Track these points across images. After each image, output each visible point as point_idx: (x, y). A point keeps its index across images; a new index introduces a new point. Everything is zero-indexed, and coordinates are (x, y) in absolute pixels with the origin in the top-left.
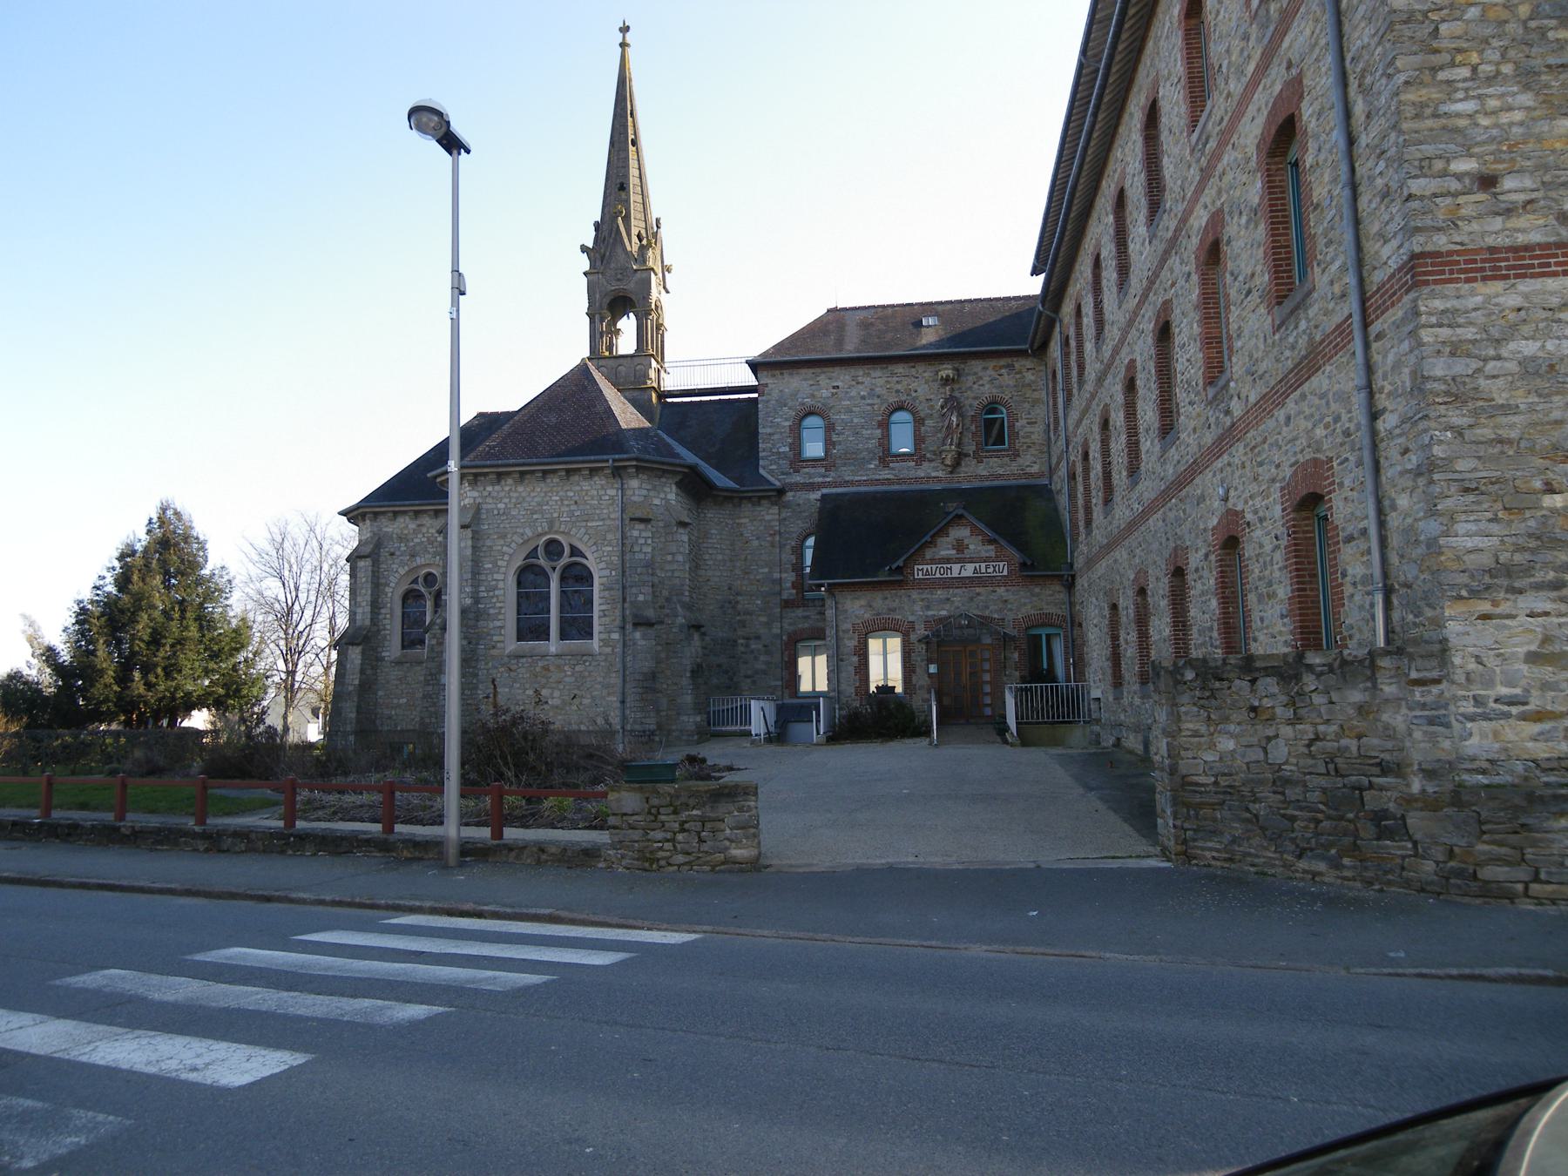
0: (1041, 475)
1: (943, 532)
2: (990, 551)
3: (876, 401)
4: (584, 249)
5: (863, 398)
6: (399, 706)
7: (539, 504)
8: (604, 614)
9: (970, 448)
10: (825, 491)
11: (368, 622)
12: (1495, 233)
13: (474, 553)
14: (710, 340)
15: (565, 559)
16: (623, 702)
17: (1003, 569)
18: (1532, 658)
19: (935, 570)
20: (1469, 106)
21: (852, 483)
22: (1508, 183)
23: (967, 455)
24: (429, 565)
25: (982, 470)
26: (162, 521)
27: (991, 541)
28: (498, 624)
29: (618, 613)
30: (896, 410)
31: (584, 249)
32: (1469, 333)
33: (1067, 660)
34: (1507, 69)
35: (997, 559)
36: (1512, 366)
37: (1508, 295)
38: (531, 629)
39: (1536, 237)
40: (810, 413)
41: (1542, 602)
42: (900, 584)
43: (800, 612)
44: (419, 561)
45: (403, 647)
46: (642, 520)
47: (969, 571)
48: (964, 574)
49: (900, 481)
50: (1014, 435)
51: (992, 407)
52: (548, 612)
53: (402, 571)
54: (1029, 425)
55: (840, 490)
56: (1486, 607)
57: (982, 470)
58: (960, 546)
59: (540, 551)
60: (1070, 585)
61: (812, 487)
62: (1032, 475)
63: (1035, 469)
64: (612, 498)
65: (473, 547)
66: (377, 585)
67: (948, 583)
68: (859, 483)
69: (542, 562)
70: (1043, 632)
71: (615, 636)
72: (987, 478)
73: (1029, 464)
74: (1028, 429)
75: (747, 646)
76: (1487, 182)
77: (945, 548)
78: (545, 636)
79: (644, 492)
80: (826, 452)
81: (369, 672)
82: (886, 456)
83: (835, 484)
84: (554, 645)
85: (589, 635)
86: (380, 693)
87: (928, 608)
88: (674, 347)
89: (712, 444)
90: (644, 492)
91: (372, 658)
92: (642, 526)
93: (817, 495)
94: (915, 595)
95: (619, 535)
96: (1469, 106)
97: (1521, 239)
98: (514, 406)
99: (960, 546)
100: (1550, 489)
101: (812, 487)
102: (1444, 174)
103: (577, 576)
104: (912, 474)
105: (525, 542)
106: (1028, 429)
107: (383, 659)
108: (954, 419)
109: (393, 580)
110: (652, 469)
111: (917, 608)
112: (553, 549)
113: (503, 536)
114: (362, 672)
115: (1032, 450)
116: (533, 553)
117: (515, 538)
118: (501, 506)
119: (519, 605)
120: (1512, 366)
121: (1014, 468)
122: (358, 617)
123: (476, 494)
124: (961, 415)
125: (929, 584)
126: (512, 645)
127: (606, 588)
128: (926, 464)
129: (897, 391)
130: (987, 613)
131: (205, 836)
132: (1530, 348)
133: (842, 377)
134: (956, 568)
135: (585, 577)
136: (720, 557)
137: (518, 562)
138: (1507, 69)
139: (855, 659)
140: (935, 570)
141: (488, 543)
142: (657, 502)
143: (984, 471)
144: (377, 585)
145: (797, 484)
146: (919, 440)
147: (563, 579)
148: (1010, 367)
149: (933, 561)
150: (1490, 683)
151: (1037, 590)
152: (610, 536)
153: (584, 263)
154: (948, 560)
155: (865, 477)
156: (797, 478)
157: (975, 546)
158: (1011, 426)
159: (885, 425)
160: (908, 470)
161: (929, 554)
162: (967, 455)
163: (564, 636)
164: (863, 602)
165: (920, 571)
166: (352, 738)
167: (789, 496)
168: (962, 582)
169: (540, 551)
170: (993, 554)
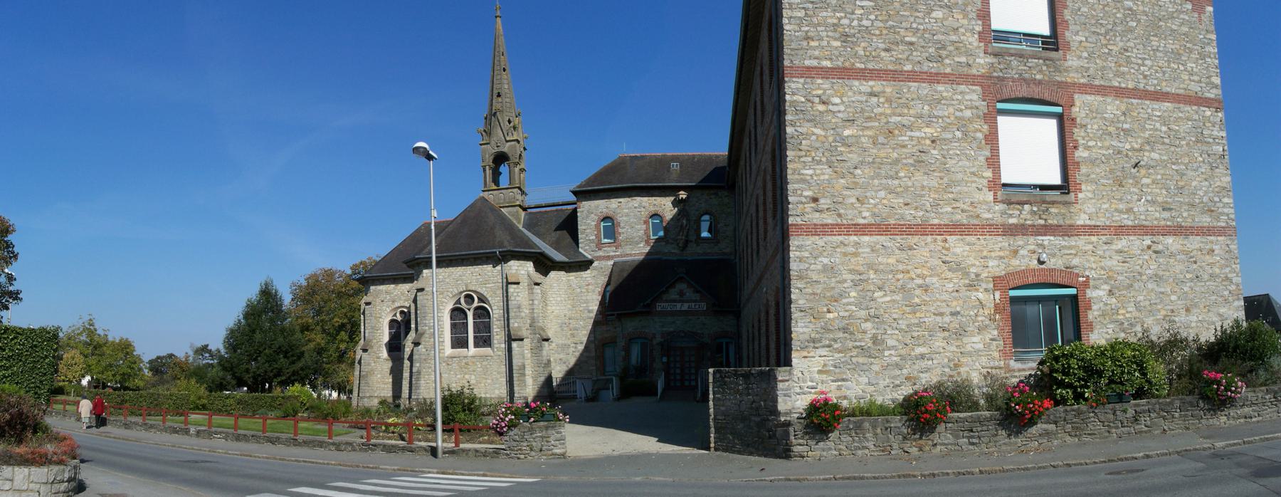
1: (672, 286)
2: (697, 296)
12: (816, 218)
15: (476, 304)
17: (704, 306)
18: (820, 372)
20: (810, 172)
22: (822, 201)
26: (266, 284)
27: (698, 292)
32: (806, 254)
34: (824, 159)
36: (819, 267)
37: (820, 241)
38: (459, 342)
39: (830, 221)
41: (824, 352)
42: (648, 313)
47: (685, 307)
52: (475, 337)
56: (805, 354)
58: (681, 293)
59: (462, 301)
60: (738, 315)
61: (609, 258)
63: (728, 250)
67: (673, 313)
70: (724, 341)
76: (815, 200)
77: (673, 294)
93: (611, 262)
96: (810, 172)
97: (825, 221)
99: (681, 293)
100: (829, 312)
101: (609, 258)
102: (801, 195)
103: (482, 313)
112: (469, 298)
116: (458, 302)
120: (819, 267)
124: (688, 220)
125: (664, 314)
126: (448, 351)
131: (333, 444)
132: (826, 261)
134: (679, 305)
137: (450, 306)
138: (824, 159)
140: (667, 307)
148: (716, 194)
150: (804, 381)
154: (675, 301)
156: (601, 253)
157: (689, 294)
161: (665, 297)
163: (476, 345)
165: (660, 306)
167: (596, 264)
169: (462, 301)
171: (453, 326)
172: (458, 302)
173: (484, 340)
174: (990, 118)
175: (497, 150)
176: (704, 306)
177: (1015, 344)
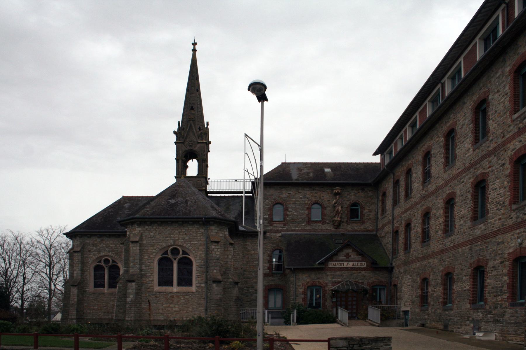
0: (372, 231)
2: (359, 258)
3: (306, 199)
4: (175, 132)
5: (301, 198)
6: (94, 309)
7: (169, 234)
8: (198, 277)
9: (345, 220)
10: (283, 233)
11: (79, 277)
13: (140, 252)
14: (229, 171)
15: (180, 256)
16: (206, 310)
17: (364, 264)
19: (337, 265)
21: (295, 231)
23: (343, 222)
24: (106, 256)
25: (349, 228)
28: (151, 279)
29: (204, 277)
30: (314, 204)
31: (175, 132)
33: (387, 297)
35: (362, 261)
40: (278, 203)
43: (270, 278)
44: (102, 254)
45: (95, 287)
46: (216, 242)
47: (351, 265)
48: (349, 266)
49: (314, 230)
50: (363, 215)
51: (355, 204)
52: (172, 275)
53: (95, 257)
54: (368, 211)
55: (290, 233)
57: (349, 228)
58: (348, 256)
61: (278, 231)
62: (369, 231)
63: (371, 228)
64: (202, 233)
65: (140, 250)
66: (83, 263)
67: (342, 269)
68: (298, 231)
69: (170, 256)
71: (203, 285)
72: (351, 231)
73: (369, 226)
74: (369, 213)
75: (248, 290)
78: (103, 286)
79: (216, 231)
80: (284, 218)
81: (81, 296)
82: (309, 221)
83: (287, 231)
84: (106, 290)
85: (191, 285)
86: (85, 304)
87: (333, 278)
88: (211, 175)
89: (229, 215)
90: (216, 231)
91: (82, 292)
92: (216, 244)
94: (328, 273)
95: (205, 247)
98: (154, 194)
99: (348, 256)
104: (320, 228)
105: (163, 248)
106: (369, 213)
107: (86, 291)
108: (340, 208)
109: (90, 260)
110: (156, 222)
111: (329, 278)
112: (175, 251)
113: (153, 246)
114: (78, 296)
115: (370, 221)
116: (166, 253)
117: (158, 246)
118: (152, 234)
119: (159, 272)
121: (362, 227)
122: (75, 275)
123: (140, 229)
125: (334, 269)
127: (199, 267)
128: (325, 225)
129: (316, 196)
130: (357, 280)
133: (292, 191)
135: (190, 263)
136: (238, 257)
137: (159, 256)
139: (303, 296)
140: (337, 265)
141: (146, 248)
142: (221, 235)
143: (351, 228)
144: (83, 263)
145: (271, 230)
146: (323, 215)
147: (179, 263)
149: (336, 261)
151: (377, 272)
152: (201, 247)
153: (174, 138)
155: (298, 230)
157: (353, 256)
158: (362, 212)
159: (309, 209)
160: (319, 226)
162: (343, 222)
163: (179, 284)
164: (307, 275)
166: (75, 321)
168: (347, 269)
169: (169, 252)
170: (361, 259)
171: (160, 271)
172: (166, 253)
173: (185, 280)
174: (448, 331)
175: (188, 148)
176: (364, 264)
177: (475, 186)
